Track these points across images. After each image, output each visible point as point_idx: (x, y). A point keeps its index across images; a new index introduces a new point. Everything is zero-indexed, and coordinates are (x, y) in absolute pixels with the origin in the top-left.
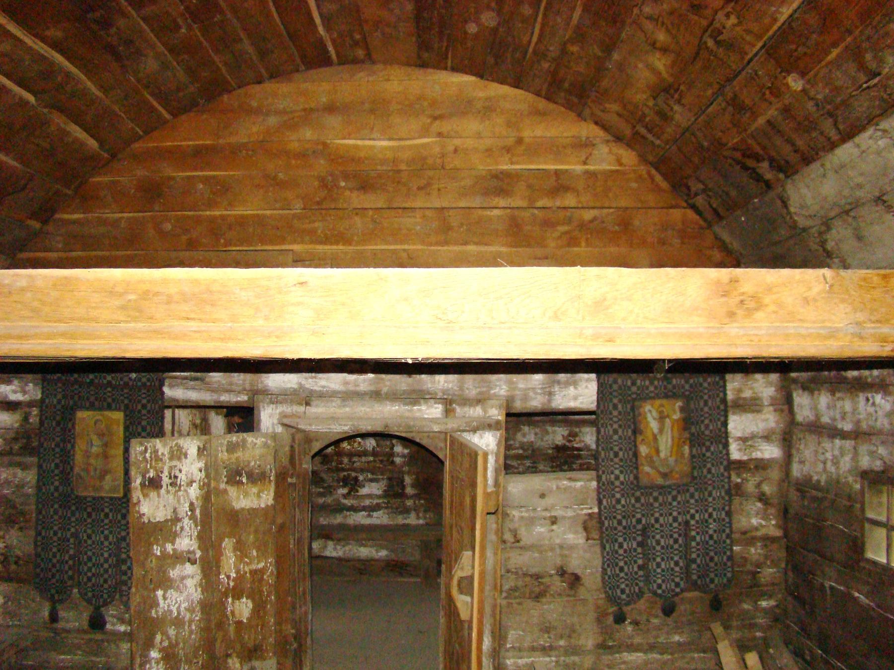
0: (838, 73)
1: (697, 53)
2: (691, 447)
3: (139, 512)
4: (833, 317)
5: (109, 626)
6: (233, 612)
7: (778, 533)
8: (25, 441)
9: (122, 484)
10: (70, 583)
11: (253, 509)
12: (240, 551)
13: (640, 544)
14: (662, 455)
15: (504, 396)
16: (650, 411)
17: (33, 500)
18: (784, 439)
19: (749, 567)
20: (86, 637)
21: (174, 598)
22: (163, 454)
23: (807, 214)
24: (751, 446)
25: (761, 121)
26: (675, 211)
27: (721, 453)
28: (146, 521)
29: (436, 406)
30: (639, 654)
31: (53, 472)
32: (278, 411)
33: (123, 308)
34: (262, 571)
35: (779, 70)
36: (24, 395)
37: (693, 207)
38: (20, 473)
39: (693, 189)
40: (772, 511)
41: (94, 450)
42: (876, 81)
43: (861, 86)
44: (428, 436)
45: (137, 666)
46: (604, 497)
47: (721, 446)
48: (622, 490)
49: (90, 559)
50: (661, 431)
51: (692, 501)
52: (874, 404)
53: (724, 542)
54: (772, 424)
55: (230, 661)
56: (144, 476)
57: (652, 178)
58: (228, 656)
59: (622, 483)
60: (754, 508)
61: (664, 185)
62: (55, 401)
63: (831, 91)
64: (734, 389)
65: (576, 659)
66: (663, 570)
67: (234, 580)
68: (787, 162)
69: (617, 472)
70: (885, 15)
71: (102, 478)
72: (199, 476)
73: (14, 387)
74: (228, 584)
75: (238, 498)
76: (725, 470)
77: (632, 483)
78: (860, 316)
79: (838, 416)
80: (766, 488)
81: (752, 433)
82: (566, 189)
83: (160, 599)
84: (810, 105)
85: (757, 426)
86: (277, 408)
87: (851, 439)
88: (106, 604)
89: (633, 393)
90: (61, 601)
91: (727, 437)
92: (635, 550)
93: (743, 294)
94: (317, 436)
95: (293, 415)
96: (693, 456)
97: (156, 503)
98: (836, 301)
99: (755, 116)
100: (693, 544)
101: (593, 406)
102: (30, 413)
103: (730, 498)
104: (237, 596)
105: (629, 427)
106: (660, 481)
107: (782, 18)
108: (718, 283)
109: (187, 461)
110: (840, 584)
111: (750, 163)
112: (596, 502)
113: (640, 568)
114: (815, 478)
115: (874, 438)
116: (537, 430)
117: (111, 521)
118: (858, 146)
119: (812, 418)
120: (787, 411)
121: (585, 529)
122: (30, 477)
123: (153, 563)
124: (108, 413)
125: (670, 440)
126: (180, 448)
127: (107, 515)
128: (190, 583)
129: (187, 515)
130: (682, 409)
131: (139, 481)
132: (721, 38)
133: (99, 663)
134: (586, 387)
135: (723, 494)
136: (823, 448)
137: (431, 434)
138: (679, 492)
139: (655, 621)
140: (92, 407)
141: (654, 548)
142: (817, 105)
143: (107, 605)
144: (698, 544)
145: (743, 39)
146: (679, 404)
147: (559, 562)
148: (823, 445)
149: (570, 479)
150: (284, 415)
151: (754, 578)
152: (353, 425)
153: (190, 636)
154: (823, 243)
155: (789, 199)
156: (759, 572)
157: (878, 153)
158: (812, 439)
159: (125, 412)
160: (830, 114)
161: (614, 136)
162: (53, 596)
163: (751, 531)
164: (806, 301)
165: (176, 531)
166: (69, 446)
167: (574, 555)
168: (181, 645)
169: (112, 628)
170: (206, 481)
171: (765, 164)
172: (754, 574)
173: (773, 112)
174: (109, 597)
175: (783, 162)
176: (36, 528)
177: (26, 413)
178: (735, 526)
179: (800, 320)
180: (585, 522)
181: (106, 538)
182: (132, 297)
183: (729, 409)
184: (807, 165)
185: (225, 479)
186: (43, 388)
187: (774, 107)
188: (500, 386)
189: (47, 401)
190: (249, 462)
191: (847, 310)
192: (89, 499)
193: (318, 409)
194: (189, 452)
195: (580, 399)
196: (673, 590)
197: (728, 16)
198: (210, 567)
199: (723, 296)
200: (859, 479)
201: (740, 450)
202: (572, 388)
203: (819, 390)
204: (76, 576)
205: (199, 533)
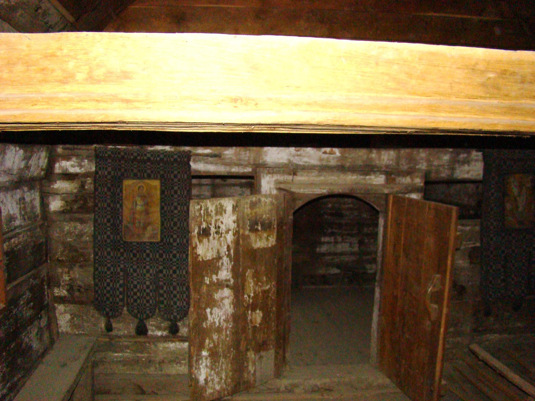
3: (196, 253)
5: (150, 333)
6: (251, 320)
9: (159, 233)
10: (121, 303)
11: (264, 248)
12: (257, 278)
15: (424, 170)
17: (91, 245)
21: (217, 314)
22: (211, 211)
28: (201, 260)
29: (381, 176)
30: (496, 335)
31: (106, 224)
32: (274, 179)
33: (483, 85)
34: (268, 291)
36: (81, 169)
38: (79, 226)
41: (139, 208)
44: (375, 197)
45: (194, 362)
49: (135, 286)
50: (520, 194)
55: (249, 353)
56: (199, 227)
58: (247, 350)
65: (459, 339)
67: (253, 298)
71: (145, 228)
72: (233, 226)
73: (72, 163)
74: (249, 301)
75: (256, 241)
83: (209, 314)
86: (273, 177)
88: (148, 317)
90: (114, 316)
94: (301, 196)
95: (285, 182)
97: (207, 246)
102: (85, 182)
104: (254, 310)
109: (227, 215)
117: (151, 259)
121: (470, 257)
122: (89, 229)
123: (204, 289)
124: (147, 181)
126: (221, 206)
127: (148, 255)
128: (227, 302)
129: (225, 254)
131: (196, 231)
133: (143, 357)
134: (475, 165)
137: (377, 195)
139: (507, 314)
140: (136, 177)
143: (149, 318)
150: (278, 182)
152: (330, 189)
153: (226, 338)
159: (161, 181)
162: (107, 314)
165: (219, 266)
166: (118, 206)
168: (221, 346)
169: (152, 333)
170: (237, 229)
174: (151, 312)
176: (94, 266)
177: (82, 182)
181: (148, 271)
182: (491, 75)
185: (249, 228)
186: (96, 163)
188: (422, 163)
189: (100, 173)
190: (262, 215)
192: (135, 244)
193: (301, 178)
194: (227, 209)
198: (238, 289)
202: (466, 165)
204: (125, 299)
205: (232, 267)
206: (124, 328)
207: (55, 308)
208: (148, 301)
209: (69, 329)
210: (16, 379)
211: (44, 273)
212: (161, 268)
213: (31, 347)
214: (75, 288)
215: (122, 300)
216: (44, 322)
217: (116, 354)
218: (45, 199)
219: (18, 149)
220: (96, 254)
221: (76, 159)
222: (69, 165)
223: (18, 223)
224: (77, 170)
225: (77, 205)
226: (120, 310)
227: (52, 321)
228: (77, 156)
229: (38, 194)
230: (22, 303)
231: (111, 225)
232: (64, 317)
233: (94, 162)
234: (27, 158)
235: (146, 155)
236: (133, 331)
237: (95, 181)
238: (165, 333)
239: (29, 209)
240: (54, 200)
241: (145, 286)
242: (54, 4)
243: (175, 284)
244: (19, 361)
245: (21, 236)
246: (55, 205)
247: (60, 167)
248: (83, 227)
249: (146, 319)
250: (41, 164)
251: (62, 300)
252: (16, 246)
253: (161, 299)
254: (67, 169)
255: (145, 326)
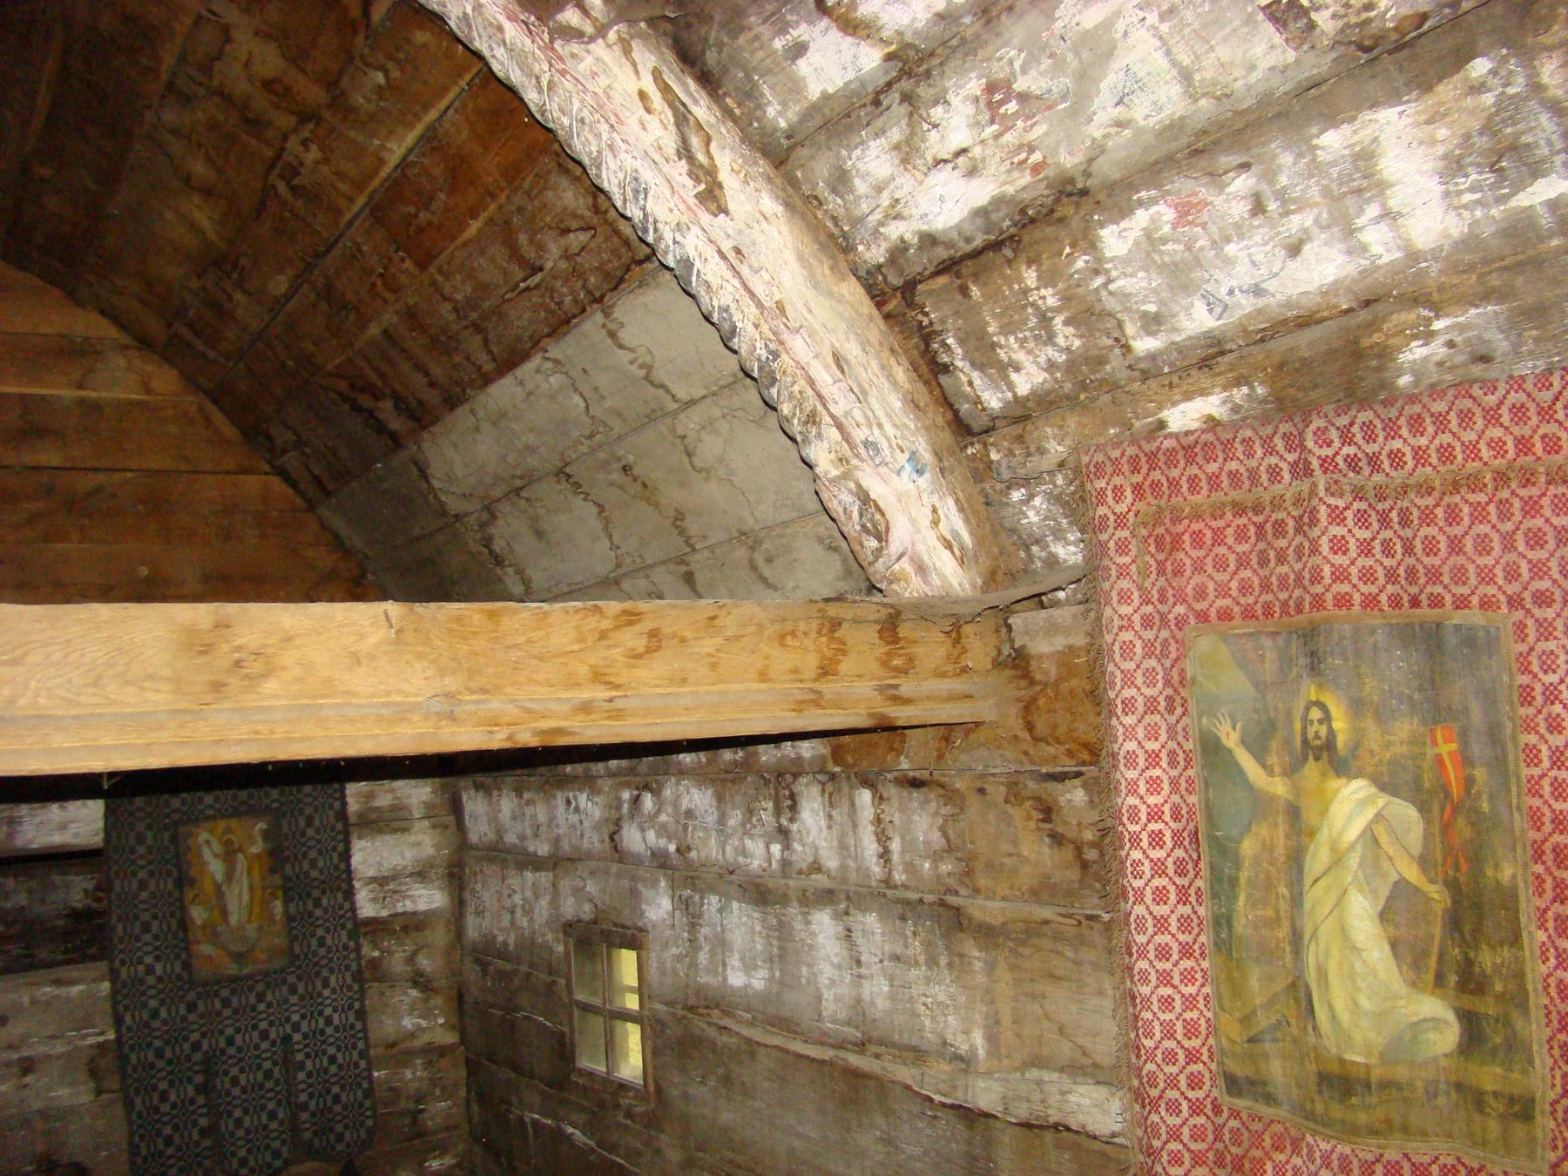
0: (482, 260)
1: (263, 203)
2: (286, 902)
4: (405, 687)
7: (450, 1038)
13: (203, 1089)
14: (233, 920)
16: (208, 842)
18: (451, 875)
19: (403, 1104)
23: (459, 492)
24: (395, 892)
25: (374, 330)
26: (249, 478)
27: (341, 907)
35: (394, 247)
37: (282, 473)
39: (279, 442)
40: (437, 1001)
42: (537, 279)
43: (517, 286)
46: (127, 1008)
47: (340, 896)
48: (162, 991)
50: (229, 875)
51: (294, 999)
52: (577, 809)
53: (356, 1065)
54: (429, 850)
57: (208, 421)
59: (160, 979)
60: (407, 1000)
61: (229, 430)
63: (475, 290)
64: (359, 794)
66: (248, 1132)
68: (421, 403)
69: (149, 960)
70: (537, 175)
76: (350, 937)
77: (179, 977)
78: (451, 683)
79: (528, 832)
80: (424, 963)
81: (394, 869)
82: (42, 432)
84: (446, 308)
85: (403, 856)
87: (547, 870)
89: (174, 811)
91: (350, 879)
92: (192, 1101)
93: (239, 649)
96: (289, 918)
98: (409, 657)
99: (363, 325)
100: (301, 1076)
101: (97, 840)
103: (361, 986)
105: (169, 874)
106: (232, 969)
107: (393, 160)
108: (191, 631)
110: (546, 1115)
111: (365, 401)
112: (111, 1021)
113: (204, 1133)
114: (500, 939)
115: (579, 865)
116: (33, 884)
118: (521, 383)
119: (492, 836)
120: (453, 828)
121: (93, 1073)
125: (246, 890)
130: (266, 835)
132: (296, 182)
135: (349, 980)
136: (509, 887)
138: (268, 986)
141: (228, 1093)
142: (456, 310)
144: (309, 1075)
145: (334, 188)
146: (261, 825)
147: (40, 1147)
148: (511, 881)
149: (59, 982)
151: (414, 1122)
154: (487, 542)
155: (429, 465)
156: (422, 1111)
157: (552, 397)
158: (491, 870)
160: (477, 328)
161: (135, 338)
163: (404, 1040)
164: (355, 659)
167: (73, 1128)
171: (387, 405)
172: (415, 1115)
173: (389, 318)
175: (414, 404)
178: (375, 1034)
179: (346, 693)
180: (92, 1060)
183: (351, 829)
184: (452, 409)
187: (391, 309)
191: (429, 673)
195: (73, 828)
196: (269, 1166)
197: (305, 143)
199: (201, 652)
200: (561, 935)
201: (374, 900)
203: (500, 790)
242: (955, 120)
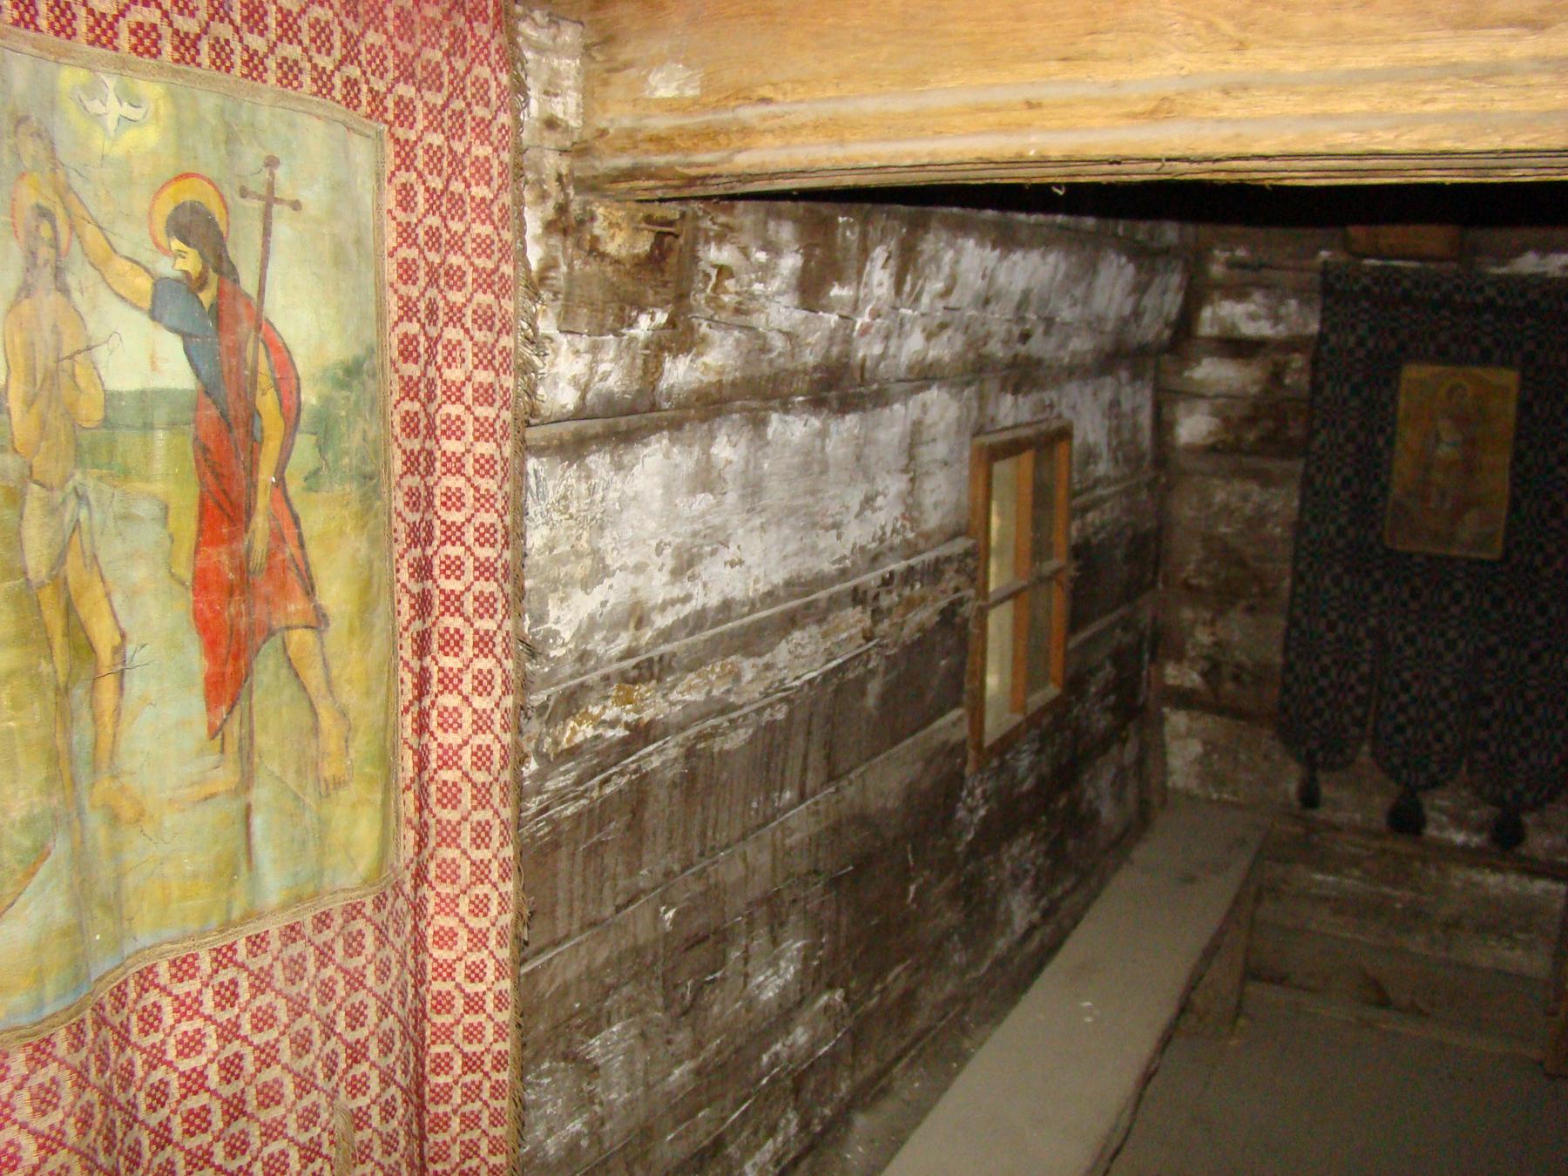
5: (1431, 831)
8: (1270, 424)
10: (1355, 731)
20: (1376, 844)
36: (1275, 325)
41: (1445, 451)
49: (1406, 687)
62: (1352, 340)
73: (1252, 308)
88: (1434, 784)
102: (1286, 364)
122: (1283, 502)
124: (1478, 371)
140: (1442, 355)
162: (1310, 756)
166: (1380, 442)
169: (1435, 833)
174: (1443, 770)
177: (1276, 364)
181: (1451, 646)
186: (1323, 310)
189: (1333, 338)
192: (1418, 559)
204: (1371, 719)
206: (1356, 803)
207: (1162, 720)
208: (1439, 738)
209: (1194, 785)
210: (1059, 891)
211: (1145, 618)
212: (1493, 640)
213: (1095, 814)
214: (1227, 671)
215: (1360, 722)
216: (1130, 753)
217: (1318, 877)
218: (1165, 410)
219: (1124, 260)
220: (1299, 578)
221: (1266, 297)
222: (1239, 315)
223: (1102, 468)
224: (1264, 329)
225: (1256, 435)
226: (1348, 751)
227: (1152, 752)
228: (1267, 287)
229: (1148, 393)
230: (1093, 689)
231: (1354, 496)
232: (1184, 745)
233: (1317, 307)
234: (1140, 289)
235: (1480, 289)
236: (1380, 821)
237: (1315, 364)
238: (1476, 840)
239: (1126, 435)
240: (1190, 413)
241: (1497, 706)
243: (1531, 695)
244: (1070, 844)
245: (1107, 505)
246: (1193, 427)
247: (1216, 319)
248: (1266, 496)
249: (1426, 788)
250: (1166, 308)
251: (1184, 699)
252: (1096, 533)
253: (1483, 735)
254: (1234, 326)
255: (1418, 807)
